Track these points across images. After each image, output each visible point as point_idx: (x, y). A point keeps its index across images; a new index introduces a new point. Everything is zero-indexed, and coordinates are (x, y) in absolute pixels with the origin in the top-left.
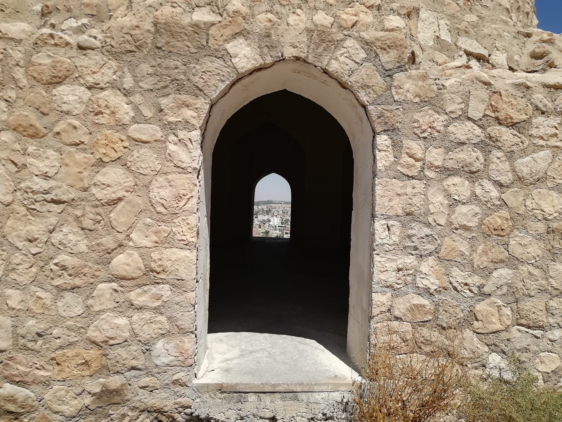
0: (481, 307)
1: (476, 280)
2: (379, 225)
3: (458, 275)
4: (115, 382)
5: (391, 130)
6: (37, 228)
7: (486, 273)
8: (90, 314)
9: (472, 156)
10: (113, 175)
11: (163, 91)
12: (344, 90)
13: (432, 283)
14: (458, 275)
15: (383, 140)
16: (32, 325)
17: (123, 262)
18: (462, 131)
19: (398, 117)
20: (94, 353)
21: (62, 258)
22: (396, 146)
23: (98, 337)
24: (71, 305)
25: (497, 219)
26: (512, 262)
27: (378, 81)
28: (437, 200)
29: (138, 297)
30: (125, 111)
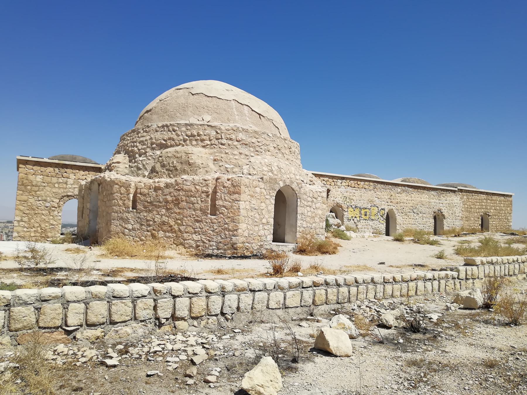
0: (311, 231)
1: (310, 226)
2: (298, 215)
3: (309, 225)
4: (262, 243)
5: (300, 198)
6: (252, 214)
7: (312, 224)
8: (259, 230)
9: (310, 203)
10: (263, 204)
11: (270, 190)
12: (381, 262)
13: (305, 226)
14: (309, 225)
15: (299, 200)
16: (251, 232)
17: (264, 221)
18: (309, 199)
19: (301, 196)
20: (259, 238)
21: (256, 220)
22: (301, 201)
23: (260, 235)
24: (256, 228)
25: (313, 215)
26: (315, 222)
27: (299, 190)
28: (306, 211)
29: (266, 227)
30: (265, 193)
